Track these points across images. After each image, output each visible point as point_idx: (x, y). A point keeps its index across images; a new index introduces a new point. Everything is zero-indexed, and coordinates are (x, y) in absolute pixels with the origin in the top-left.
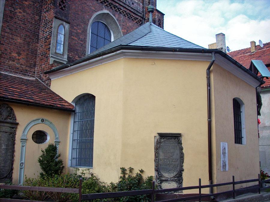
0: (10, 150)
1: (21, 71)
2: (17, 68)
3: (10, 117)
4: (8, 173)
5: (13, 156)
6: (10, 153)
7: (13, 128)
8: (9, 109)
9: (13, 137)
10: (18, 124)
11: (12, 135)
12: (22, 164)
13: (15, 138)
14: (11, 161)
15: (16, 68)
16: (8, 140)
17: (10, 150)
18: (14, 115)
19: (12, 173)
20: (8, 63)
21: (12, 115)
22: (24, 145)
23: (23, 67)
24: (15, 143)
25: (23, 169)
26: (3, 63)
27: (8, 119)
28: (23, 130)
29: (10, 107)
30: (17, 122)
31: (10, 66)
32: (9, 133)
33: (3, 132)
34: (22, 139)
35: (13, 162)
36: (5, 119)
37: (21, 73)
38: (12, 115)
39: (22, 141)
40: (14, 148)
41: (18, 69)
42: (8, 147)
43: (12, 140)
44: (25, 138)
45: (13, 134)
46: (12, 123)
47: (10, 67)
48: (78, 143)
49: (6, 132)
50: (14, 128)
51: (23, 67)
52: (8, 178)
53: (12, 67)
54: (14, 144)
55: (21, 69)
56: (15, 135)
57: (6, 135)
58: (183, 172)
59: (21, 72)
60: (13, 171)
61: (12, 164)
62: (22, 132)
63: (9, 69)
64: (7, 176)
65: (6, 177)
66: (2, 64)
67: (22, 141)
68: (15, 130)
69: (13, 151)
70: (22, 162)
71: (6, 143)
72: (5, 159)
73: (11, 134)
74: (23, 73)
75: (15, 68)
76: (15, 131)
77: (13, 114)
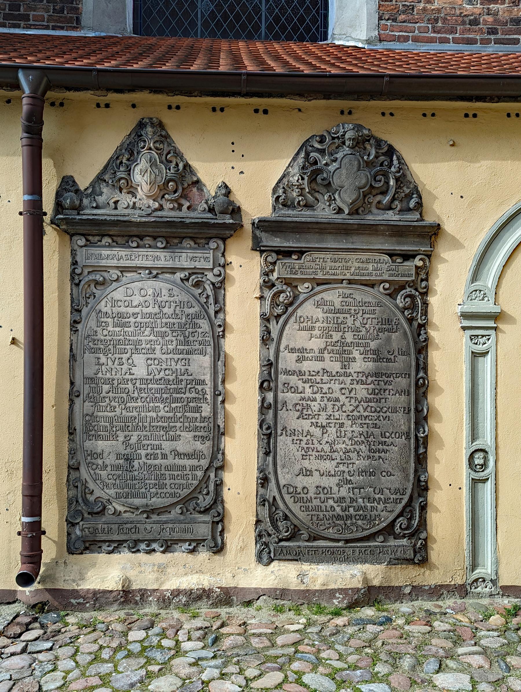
0: (402, 382)
1: (493, 31)
2: (471, 23)
3: (379, 198)
4: (399, 507)
5: (418, 411)
6: (403, 398)
7: (407, 257)
8: (373, 152)
9: (413, 307)
10: (434, 232)
11: (413, 296)
12: (481, 455)
13: (425, 313)
14: (408, 438)
15: (467, 19)
16: (387, 325)
17: (402, 382)
18: (403, 178)
19: (423, 508)
20: (424, 9)
21: (392, 182)
22: (480, 348)
23: (496, 14)
24: (426, 340)
25: (489, 486)
26: (404, 12)
27: (375, 211)
28: (470, 264)
29: (379, 143)
30: (429, 219)
31: (436, 20)
32: (387, 285)
33: (350, 282)
34: (465, 316)
35: (425, 445)
36: (354, 212)
37: (492, 37)
38: (392, 182)
39: (467, 323)
40: (422, 366)
41: (475, 22)
42: (389, 360)
43: (406, 326)
44: (487, 306)
45: (408, 290)
46: (398, 232)
47: (440, 24)
48: (183, 220)
49: (372, 285)
50: (414, 257)
51: (496, 14)
52: (404, 537)
53: (445, 20)
54: (421, 348)
55: (490, 19)
56: (425, 294)
57: (370, 299)
58: (27, 197)
59: (489, 33)
60: (430, 492)
61: (421, 460)
62: (467, 276)
63: (434, 32)
64: (392, 524)
65: (389, 530)
66: (402, 17)
67: (467, 323)
68: (421, 264)
69: (421, 388)
70: (478, 444)
71: (373, 345)
72: (377, 431)
73: (403, 288)
74: (499, 36)
75: (463, 23)
76: (424, 274)
77: (397, 180)
